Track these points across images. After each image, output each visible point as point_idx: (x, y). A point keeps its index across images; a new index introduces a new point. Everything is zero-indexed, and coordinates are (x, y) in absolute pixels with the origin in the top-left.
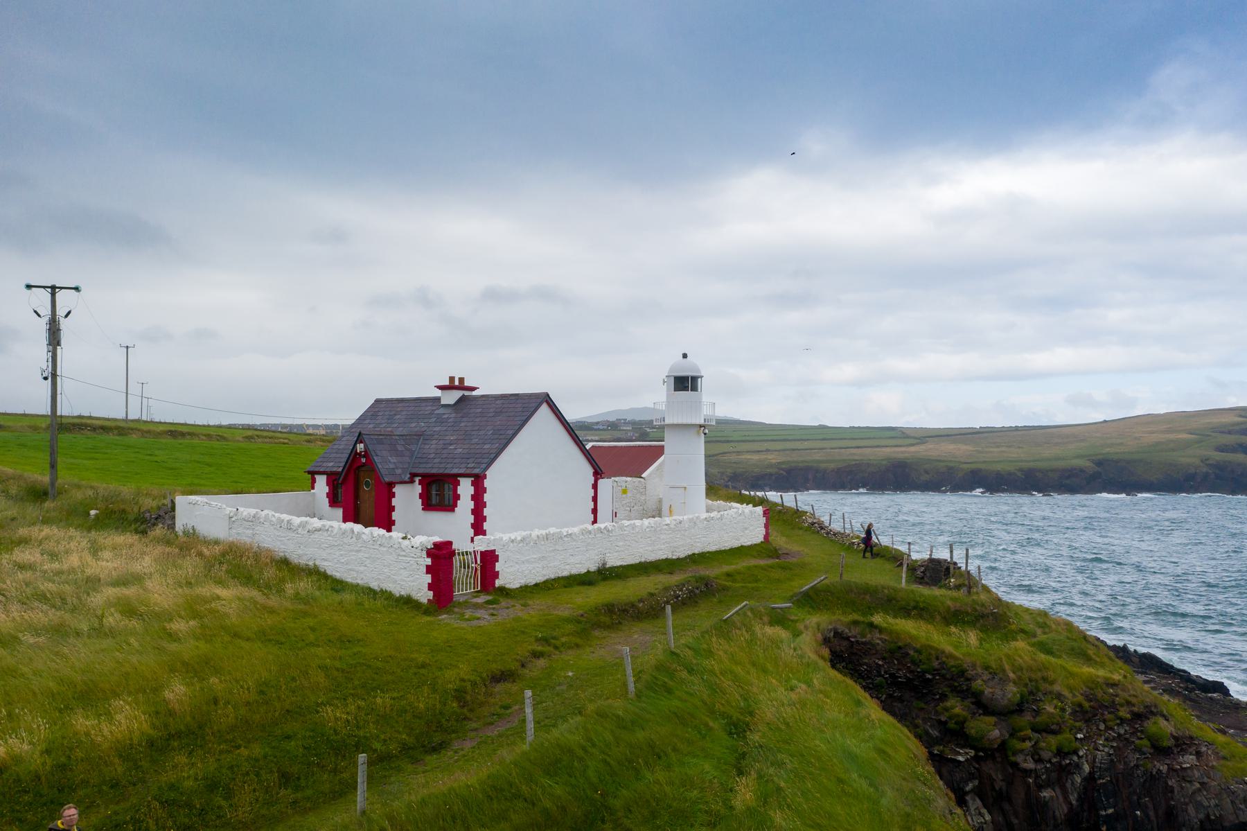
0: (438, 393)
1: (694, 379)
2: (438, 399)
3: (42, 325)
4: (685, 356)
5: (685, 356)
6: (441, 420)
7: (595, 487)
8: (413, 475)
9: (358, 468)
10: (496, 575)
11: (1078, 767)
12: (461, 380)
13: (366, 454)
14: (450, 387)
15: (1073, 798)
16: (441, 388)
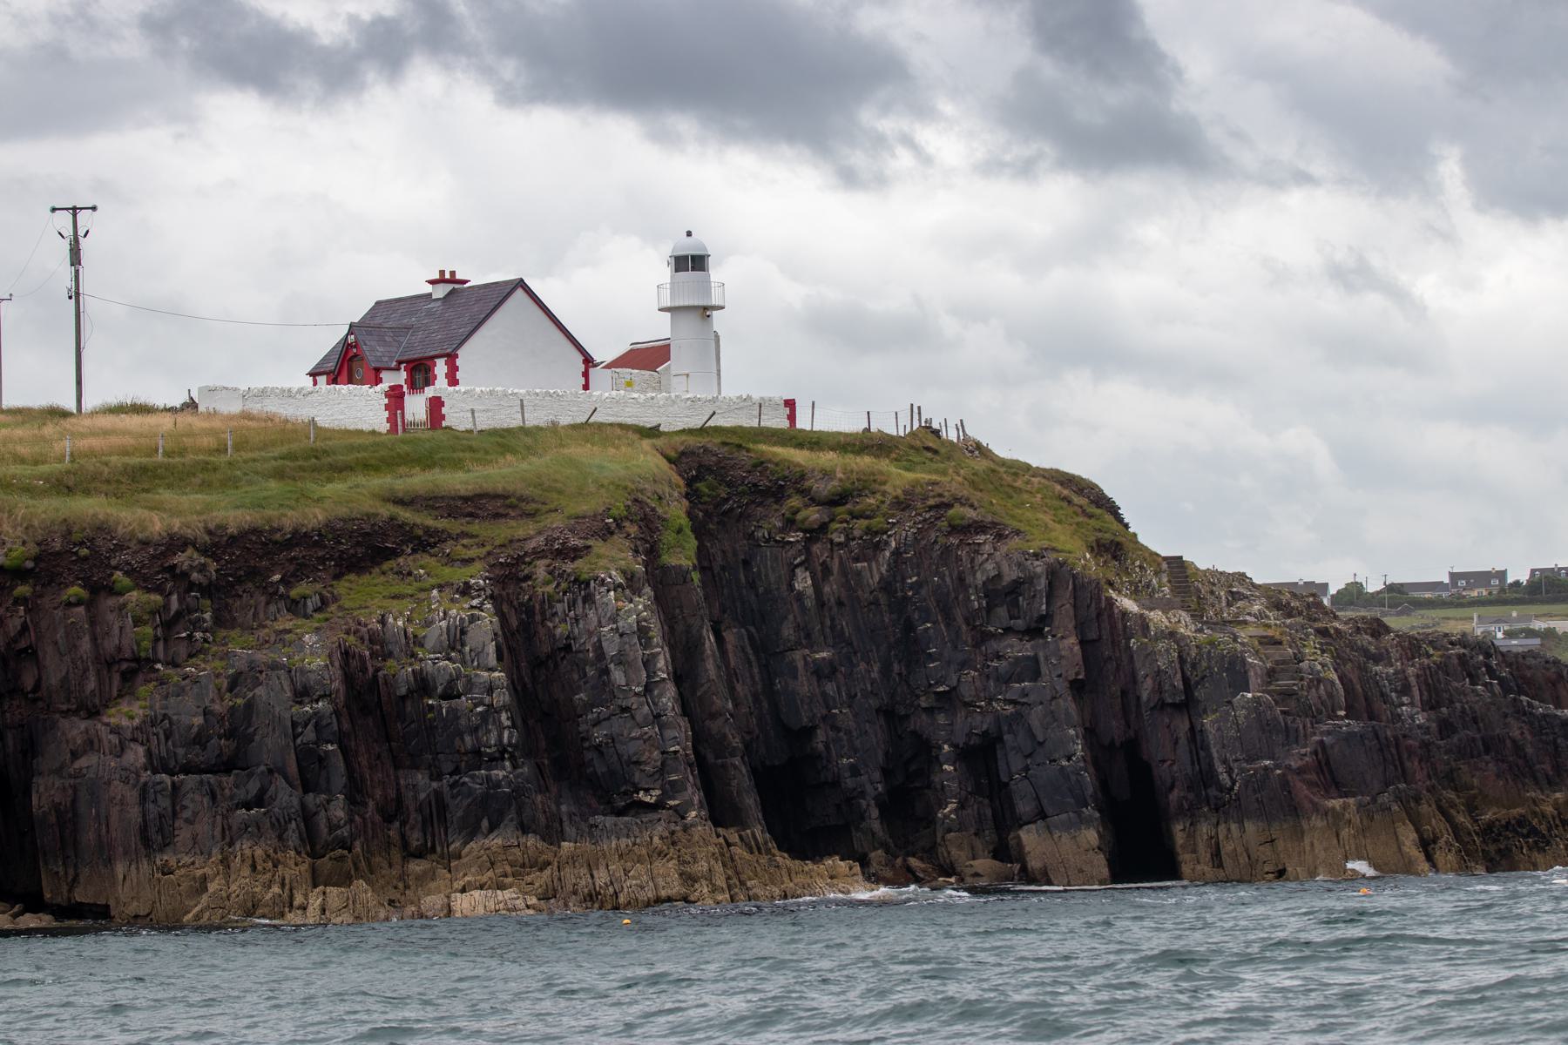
0: (429, 289)
2: (430, 295)
3: (65, 246)
4: (689, 234)
5: (689, 234)
6: (430, 313)
7: (586, 375)
8: (400, 363)
9: (351, 359)
10: (443, 417)
11: (887, 543)
12: (453, 273)
14: (441, 280)
15: (883, 569)
16: (432, 282)
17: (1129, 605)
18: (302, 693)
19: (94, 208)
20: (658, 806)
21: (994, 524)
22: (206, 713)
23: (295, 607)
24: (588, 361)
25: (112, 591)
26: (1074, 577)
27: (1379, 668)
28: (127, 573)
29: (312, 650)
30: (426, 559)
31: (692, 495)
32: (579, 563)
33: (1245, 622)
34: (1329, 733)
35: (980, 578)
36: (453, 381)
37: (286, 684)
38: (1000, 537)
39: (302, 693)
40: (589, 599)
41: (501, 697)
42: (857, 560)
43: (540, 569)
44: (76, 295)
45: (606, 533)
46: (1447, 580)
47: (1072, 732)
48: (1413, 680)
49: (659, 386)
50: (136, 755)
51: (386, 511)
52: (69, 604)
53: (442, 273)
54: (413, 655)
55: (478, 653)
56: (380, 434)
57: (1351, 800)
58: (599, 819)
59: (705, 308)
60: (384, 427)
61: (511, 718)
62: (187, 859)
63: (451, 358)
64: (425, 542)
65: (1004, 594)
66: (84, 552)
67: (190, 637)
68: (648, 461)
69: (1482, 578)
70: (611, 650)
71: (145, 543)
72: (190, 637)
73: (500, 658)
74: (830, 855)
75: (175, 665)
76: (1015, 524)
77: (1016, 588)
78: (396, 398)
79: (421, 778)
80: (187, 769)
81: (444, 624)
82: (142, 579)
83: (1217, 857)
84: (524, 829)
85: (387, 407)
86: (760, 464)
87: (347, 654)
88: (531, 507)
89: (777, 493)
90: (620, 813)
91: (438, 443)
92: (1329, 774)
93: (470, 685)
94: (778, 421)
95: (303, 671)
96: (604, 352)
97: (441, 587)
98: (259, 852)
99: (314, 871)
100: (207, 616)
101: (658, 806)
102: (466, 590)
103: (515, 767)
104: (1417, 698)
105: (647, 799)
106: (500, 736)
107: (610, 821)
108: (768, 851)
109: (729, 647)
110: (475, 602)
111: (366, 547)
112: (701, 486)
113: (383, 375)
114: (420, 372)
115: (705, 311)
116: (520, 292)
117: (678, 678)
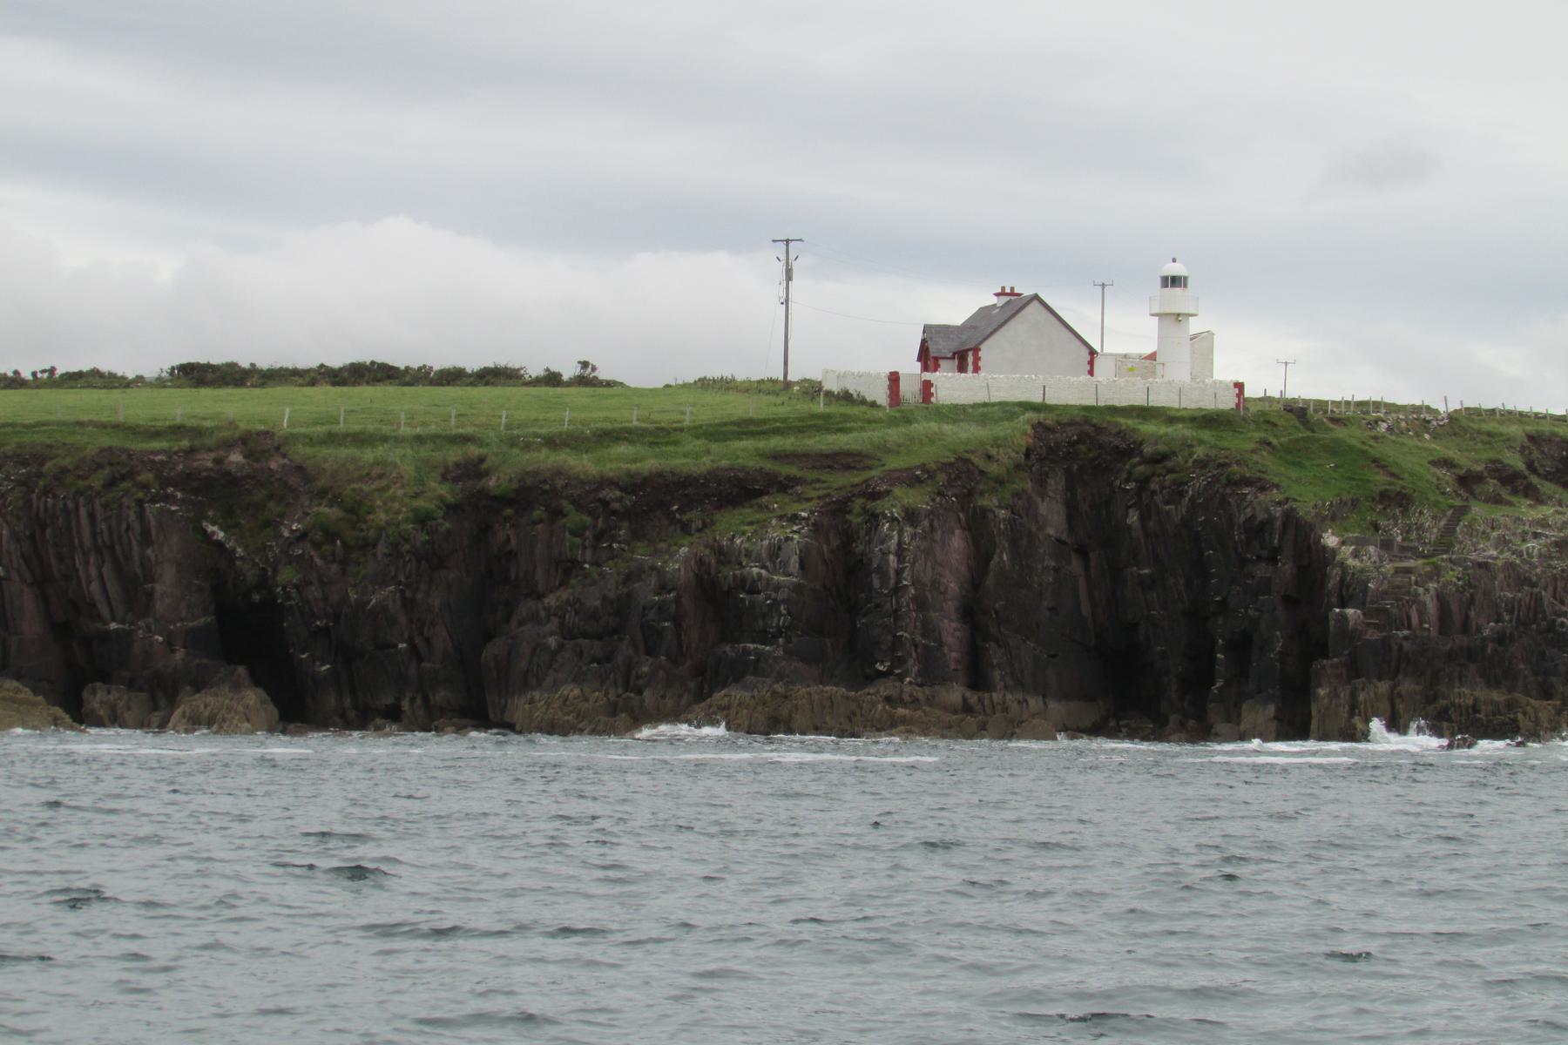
7: (1091, 363)
16: (997, 295)
20: (888, 673)
21: (1260, 479)
23: (685, 528)
29: (679, 559)
30: (780, 497)
35: (1243, 518)
38: (1263, 489)
39: (663, 588)
42: (1168, 503)
52: (535, 523)
55: (785, 563)
63: (976, 350)
64: (784, 486)
65: (1258, 530)
66: (547, 487)
72: (610, 546)
76: (1276, 480)
82: (577, 504)
86: (1121, 434)
87: (701, 562)
89: (1127, 453)
101: (888, 673)
102: (794, 518)
109: (1092, 564)
111: (740, 490)
116: (1035, 304)
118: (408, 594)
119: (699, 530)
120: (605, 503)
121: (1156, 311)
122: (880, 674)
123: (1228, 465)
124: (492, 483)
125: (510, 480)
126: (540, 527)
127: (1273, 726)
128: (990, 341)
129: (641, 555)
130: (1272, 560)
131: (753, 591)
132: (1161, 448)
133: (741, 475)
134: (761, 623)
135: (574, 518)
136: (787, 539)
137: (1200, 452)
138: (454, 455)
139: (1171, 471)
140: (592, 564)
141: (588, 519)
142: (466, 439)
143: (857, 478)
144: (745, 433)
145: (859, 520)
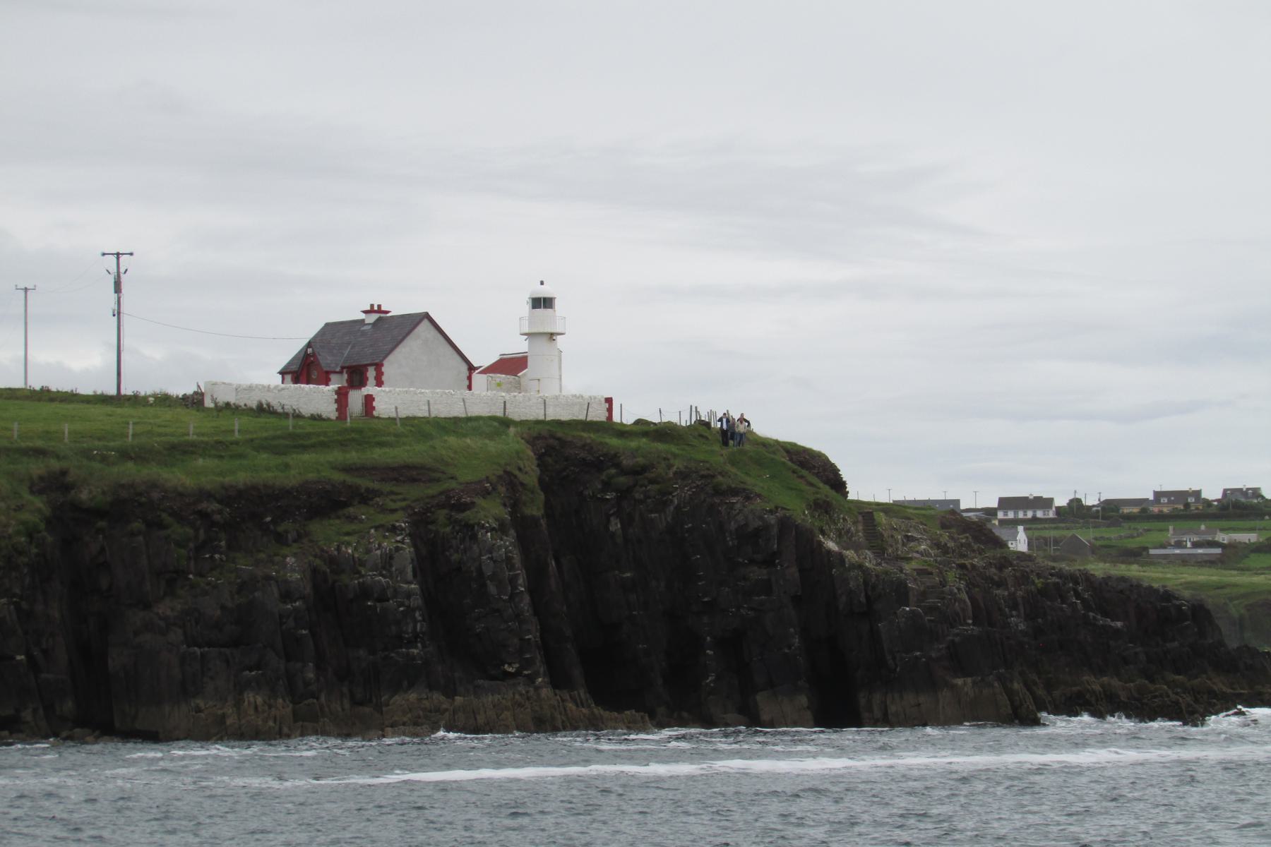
0: (363, 316)
1: (534, 307)
4: (542, 283)
5: (542, 283)
6: (364, 333)
7: (470, 378)
11: (672, 501)
12: (379, 306)
13: (314, 355)
15: (669, 519)
16: (365, 312)
17: (831, 545)
18: (286, 596)
19: (131, 254)
22: (223, 608)
23: (281, 539)
24: (471, 368)
25: (161, 526)
26: (797, 527)
27: (998, 592)
28: (170, 515)
29: (292, 567)
31: (542, 464)
32: (468, 513)
33: (911, 559)
34: (957, 635)
35: (733, 526)
36: (379, 383)
37: (275, 590)
38: (748, 498)
40: (474, 537)
41: (417, 601)
42: (651, 512)
43: (442, 514)
44: (118, 314)
45: (486, 494)
46: (1151, 498)
47: (792, 630)
48: (1020, 600)
49: (518, 387)
50: (176, 635)
51: (338, 477)
53: (372, 306)
54: (359, 572)
55: (402, 571)
56: (329, 419)
57: (969, 680)
58: (481, 682)
59: (552, 334)
60: (334, 415)
61: (422, 615)
62: (211, 703)
63: (378, 367)
64: (365, 498)
65: (752, 536)
66: (144, 499)
67: (212, 557)
68: (513, 442)
69: (1180, 496)
70: (488, 572)
71: (181, 495)
72: (212, 557)
73: (415, 576)
74: (629, 709)
75: (202, 575)
77: (757, 533)
78: (342, 396)
79: (362, 653)
80: (210, 644)
81: (378, 552)
83: (885, 714)
84: (431, 687)
85: (336, 401)
87: (315, 571)
88: (437, 475)
90: (493, 678)
91: (370, 430)
92: (959, 661)
93: (396, 592)
94: (598, 415)
95: (286, 582)
96: (483, 359)
97: (376, 528)
98: (259, 700)
99: (295, 713)
100: (223, 543)
102: (394, 529)
103: (424, 646)
104: (1022, 611)
105: (510, 670)
106: (415, 627)
107: (486, 683)
108: (589, 706)
110: (399, 538)
111: (328, 501)
112: (549, 460)
113: (333, 377)
114: (356, 376)
115: (551, 336)
116: (426, 322)
117: (531, 591)
118: (24, 605)
119: (295, 541)
120: (204, 515)
121: (527, 331)
122: (507, 675)
123: (713, 476)
124: (84, 496)
125: (104, 493)
126: (141, 538)
127: (809, 715)
128: (391, 357)
129: (244, 565)
130: (769, 562)
131: (382, 599)
132: (640, 460)
133: (328, 487)
134: (393, 628)
135: (179, 530)
136: (397, 549)
137: (678, 464)
138: (37, 468)
139: (652, 482)
140: (195, 575)
141: (189, 531)
142: (39, 453)
143: (433, 490)
144: (295, 447)
145: (448, 529)
